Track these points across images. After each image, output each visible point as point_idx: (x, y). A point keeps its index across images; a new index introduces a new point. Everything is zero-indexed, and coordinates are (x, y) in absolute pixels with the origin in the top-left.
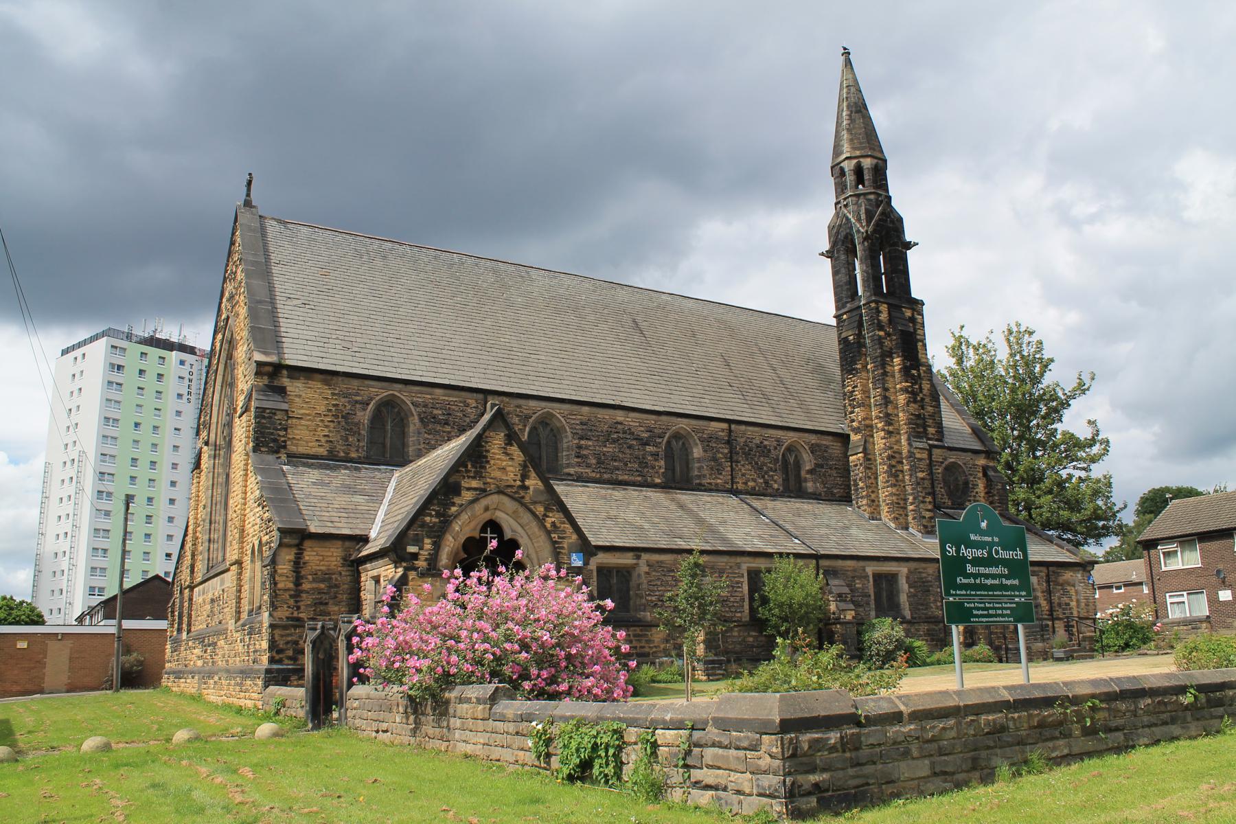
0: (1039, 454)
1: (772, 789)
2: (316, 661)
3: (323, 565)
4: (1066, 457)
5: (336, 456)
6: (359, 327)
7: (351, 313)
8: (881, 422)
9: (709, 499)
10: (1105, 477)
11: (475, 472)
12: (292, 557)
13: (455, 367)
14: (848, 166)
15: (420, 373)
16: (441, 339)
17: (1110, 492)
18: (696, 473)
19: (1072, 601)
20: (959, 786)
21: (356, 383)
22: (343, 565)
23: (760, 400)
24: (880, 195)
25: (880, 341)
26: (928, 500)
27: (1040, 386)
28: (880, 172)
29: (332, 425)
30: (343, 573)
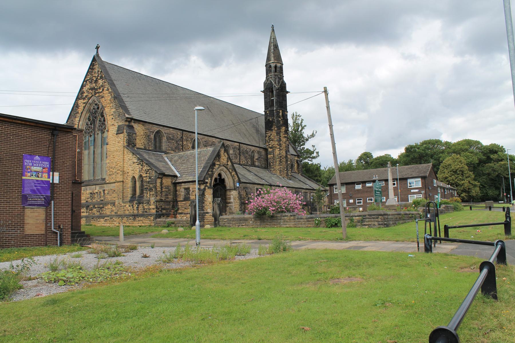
12: (160, 181)
14: (273, 65)
21: (151, 125)
28: (281, 68)
29: (145, 139)
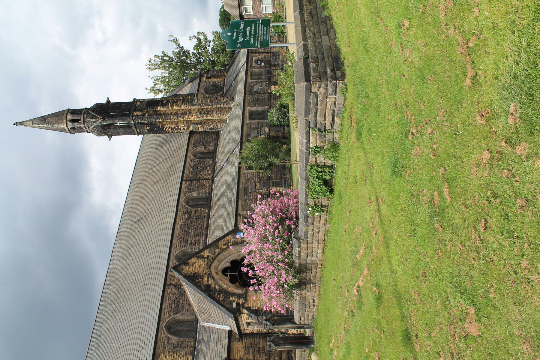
0: (202, 61)
1: (333, 87)
2: (284, 344)
3: (242, 350)
4: (204, 49)
5: (192, 351)
6: (132, 344)
7: (126, 349)
9: (215, 189)
10: (213, 34)
11: (200, 279)
13: (153, 299)
14: (70, 125)
15: (155, 314)
16: (140, 307)
17: (220, 32)
18: (204, 195)
20: (332, 27)
21: (159, 343)
22: (242, 341)
23: (173, 168)
24: (85, 112)
26: (219, 99)
27: (174, 58)
29: (178, 354)
30: (245, 341)
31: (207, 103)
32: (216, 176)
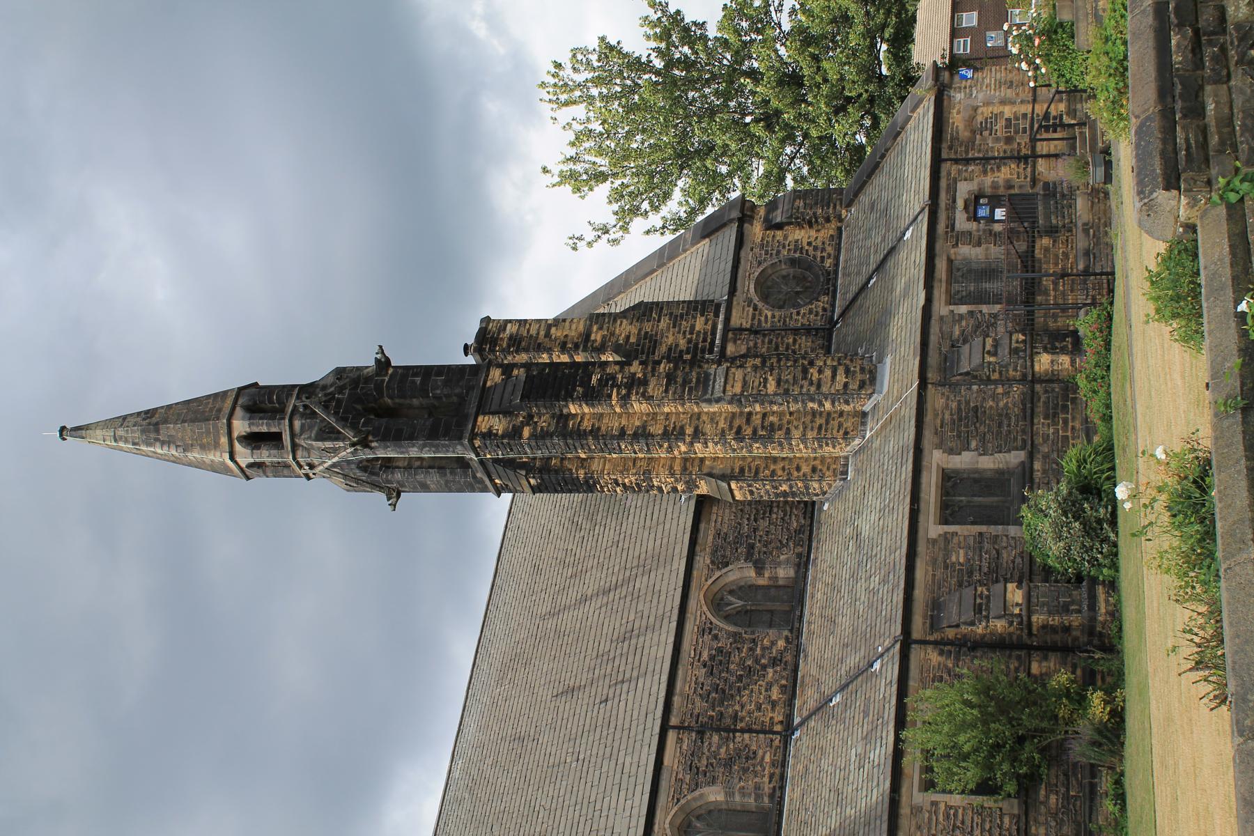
8: (679, 447)
14: (245, 456)
18: (752, 800)
19: (1002, 113)
25: (540, 437)
26: (816, 376)
31: (767, 395)
32: (801, 724)
